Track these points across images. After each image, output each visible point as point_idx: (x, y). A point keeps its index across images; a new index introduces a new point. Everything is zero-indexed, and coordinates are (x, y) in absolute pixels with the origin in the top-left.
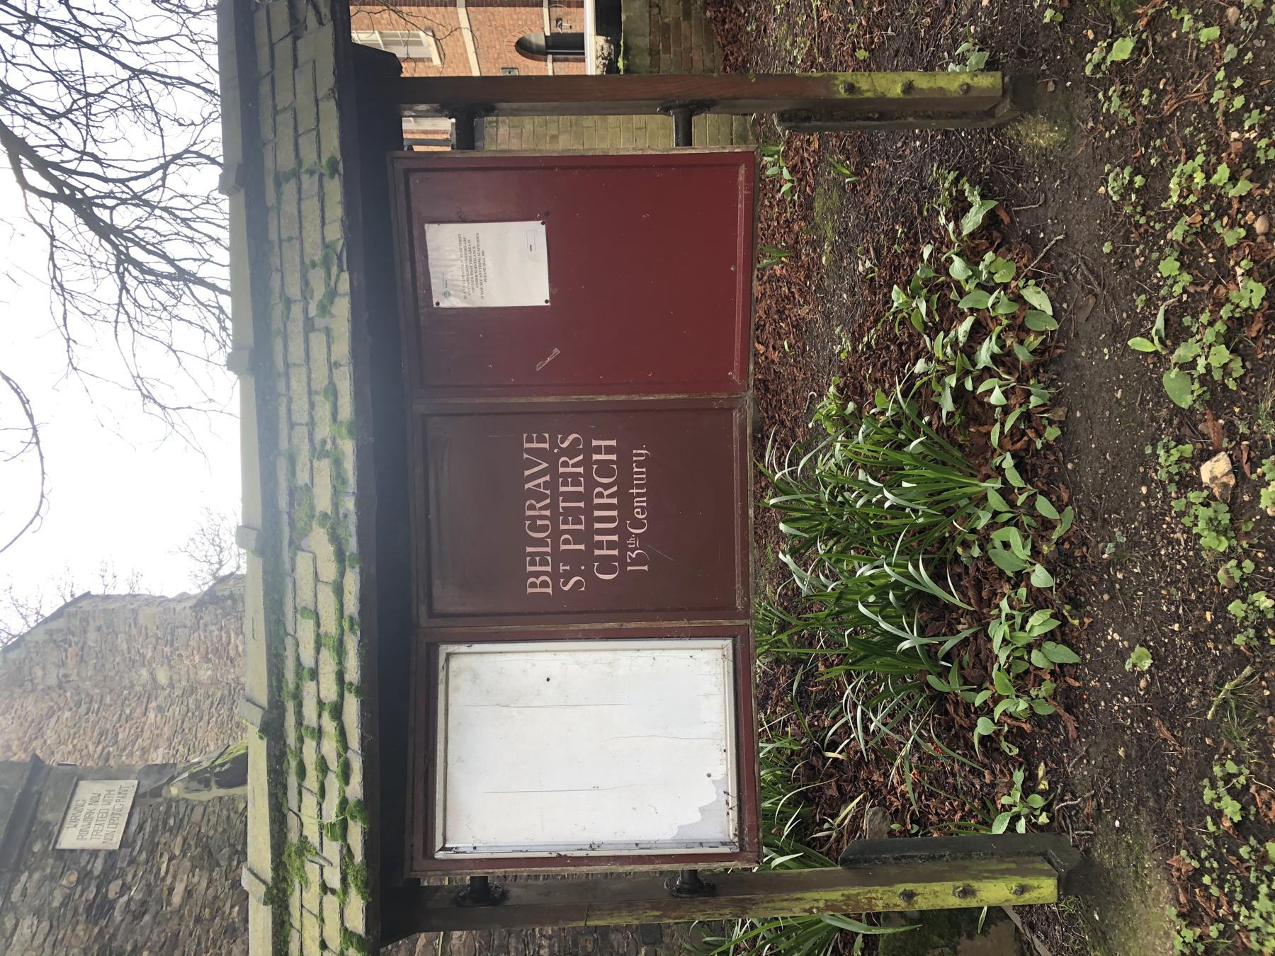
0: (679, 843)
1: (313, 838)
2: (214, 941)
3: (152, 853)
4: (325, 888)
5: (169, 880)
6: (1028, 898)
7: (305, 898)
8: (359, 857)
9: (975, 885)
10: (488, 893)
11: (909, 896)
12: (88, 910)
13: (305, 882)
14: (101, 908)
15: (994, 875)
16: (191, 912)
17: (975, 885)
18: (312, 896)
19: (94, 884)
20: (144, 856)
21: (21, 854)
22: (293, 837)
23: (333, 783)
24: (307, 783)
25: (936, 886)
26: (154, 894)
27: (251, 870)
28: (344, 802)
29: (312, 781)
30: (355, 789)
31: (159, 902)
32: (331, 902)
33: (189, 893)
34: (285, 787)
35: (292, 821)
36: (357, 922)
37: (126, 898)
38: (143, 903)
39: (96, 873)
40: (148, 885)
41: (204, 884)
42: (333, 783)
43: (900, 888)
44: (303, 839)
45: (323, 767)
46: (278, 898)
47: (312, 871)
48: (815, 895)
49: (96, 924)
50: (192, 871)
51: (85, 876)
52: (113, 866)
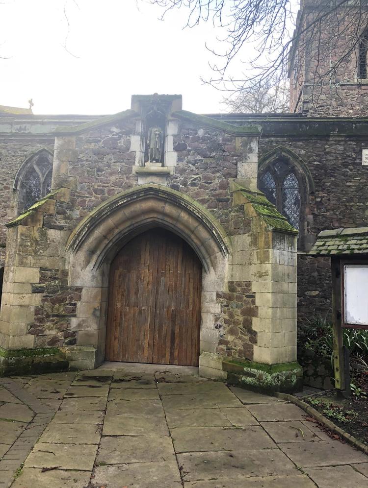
0: (346, 312)
1: (348, 243)
2: (336, 196)
3: (360, 174)
4: (339, 245)
5: (353, 181)
6: (336, 382)
7: (337, 241)
8: (344, 253)
9: (339, 371)
10: (338, 277)
11: (337, 358)
12: (346, 162)
13: (340, 241)
14: (346, 165)
15: (341, 376)
16: (344, 188)
17: (339, 371)
18: (337, 243)
19: (353, 162)
20: (360, 172)
21: (361, 140)
22: (349, 238)
23: (357, 247)
24: (358, 241)
25: (338, 363)
26: (348, 178)
27: (343, 230)
28: (353, 249)
29: (359, 242)
30: (356, 252)
31: (348, 179)
32: (335, 247)
33: (349, 186)
34: (358, 236)
35: (352, 238)
36: (333, 252)
37: (348, 170)
38: (347, 176)
39: (355, 161)
40: (352, 176)
41: (352, 190)
42: (357, 247)
43: (338, 356)
44: (348, 241)
45: (361, 244)
46: (337, 236)
47: (342, 243)
48: (337, 338)
49: (342, 165)
50: (356, 186)
51: (355, 159)
52: (357, 165)
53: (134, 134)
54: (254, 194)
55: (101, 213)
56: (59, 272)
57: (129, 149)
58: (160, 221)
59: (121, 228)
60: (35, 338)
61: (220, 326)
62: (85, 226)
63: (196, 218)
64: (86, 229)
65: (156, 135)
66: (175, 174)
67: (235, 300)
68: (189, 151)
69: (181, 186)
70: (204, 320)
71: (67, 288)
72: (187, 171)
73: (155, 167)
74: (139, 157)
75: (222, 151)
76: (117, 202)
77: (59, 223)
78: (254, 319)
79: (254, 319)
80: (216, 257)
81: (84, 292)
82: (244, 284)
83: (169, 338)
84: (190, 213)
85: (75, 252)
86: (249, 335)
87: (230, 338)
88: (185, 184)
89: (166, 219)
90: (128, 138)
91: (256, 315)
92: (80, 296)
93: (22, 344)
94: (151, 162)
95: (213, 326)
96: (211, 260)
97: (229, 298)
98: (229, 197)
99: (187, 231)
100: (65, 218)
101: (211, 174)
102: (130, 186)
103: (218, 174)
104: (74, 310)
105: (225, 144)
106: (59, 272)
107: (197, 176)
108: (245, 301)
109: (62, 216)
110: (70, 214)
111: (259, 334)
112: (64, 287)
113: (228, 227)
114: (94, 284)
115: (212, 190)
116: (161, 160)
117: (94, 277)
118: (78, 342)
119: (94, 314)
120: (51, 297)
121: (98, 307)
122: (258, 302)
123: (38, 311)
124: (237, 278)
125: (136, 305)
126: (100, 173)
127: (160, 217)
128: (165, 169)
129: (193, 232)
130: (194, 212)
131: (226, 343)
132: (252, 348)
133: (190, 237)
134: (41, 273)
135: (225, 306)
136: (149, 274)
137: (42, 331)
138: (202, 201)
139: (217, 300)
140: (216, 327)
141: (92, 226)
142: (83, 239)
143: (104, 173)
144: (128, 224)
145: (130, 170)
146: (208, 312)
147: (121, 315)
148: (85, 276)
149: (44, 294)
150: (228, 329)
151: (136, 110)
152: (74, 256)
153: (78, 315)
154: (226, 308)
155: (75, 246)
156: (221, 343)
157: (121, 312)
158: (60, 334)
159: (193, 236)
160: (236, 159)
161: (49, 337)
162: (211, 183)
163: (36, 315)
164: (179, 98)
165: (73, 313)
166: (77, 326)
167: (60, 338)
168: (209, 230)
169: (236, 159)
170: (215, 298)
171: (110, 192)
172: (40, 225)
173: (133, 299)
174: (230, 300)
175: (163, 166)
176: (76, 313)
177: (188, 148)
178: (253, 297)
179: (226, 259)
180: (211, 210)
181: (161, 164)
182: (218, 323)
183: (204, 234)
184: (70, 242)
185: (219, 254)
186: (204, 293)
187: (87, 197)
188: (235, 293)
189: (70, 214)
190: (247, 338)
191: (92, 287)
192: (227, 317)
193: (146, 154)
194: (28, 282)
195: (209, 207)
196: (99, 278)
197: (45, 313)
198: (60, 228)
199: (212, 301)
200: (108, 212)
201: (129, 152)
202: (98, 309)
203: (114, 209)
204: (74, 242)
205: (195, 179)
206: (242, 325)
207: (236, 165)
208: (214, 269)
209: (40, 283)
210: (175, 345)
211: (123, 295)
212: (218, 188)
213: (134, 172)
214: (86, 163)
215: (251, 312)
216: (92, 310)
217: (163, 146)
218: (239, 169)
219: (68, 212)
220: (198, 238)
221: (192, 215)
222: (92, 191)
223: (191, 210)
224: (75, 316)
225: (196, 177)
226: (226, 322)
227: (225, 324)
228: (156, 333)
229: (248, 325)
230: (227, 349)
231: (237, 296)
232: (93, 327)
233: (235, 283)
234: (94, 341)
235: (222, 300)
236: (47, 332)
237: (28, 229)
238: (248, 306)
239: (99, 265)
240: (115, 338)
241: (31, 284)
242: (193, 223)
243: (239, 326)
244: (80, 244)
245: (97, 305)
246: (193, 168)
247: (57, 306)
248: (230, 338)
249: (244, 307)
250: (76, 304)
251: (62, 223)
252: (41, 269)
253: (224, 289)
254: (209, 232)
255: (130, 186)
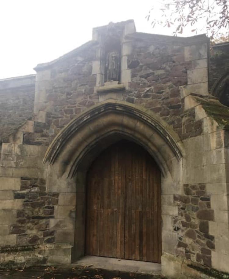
53: (95, 60)
54: (205, 98)
55: (71, 129)
56: (38, 181)
57: (90, 73)
58: (121, 132)
59: (89, 141)
60: (17, 237)
61: (178, 229)
62: (58, 140)
63: (154, 129)
64: (59, 144)
65: (112, 57)
66: (130, 89)
67: (190, 203)
68: (142, 67)
69: (135, 99)
70: (164, 222)
71: (46, 194)
72: (141, 85)
73: (114, 85)
74: (99, 79)
75: (171, 62)
76: (82, 118)
77: (38, 140)
78: (210, 223)
79: (210, 223)
80: (171, 162)
81: (60, 198)
82: (198, 186)
83: (137, 236)
84: (145, 123)
85: (52, 163)
86: (207, 240)
87: (188, 241)
88: (138, 96)
89: (126, 130)
90: (90, 64)
91: (212, 219)
92: (57, 201)
93: (5, 243)
94: (109, 81)
95: (172, 228)
96: (167, 165)
97: (185, 201)
98: (180, 103)
99: (144, 140)
100: (43, 136)
101: (162, 84)
102: (93, 104)
103: (169, 84)
104: (52, 213)
105: (175, 55)
106: (38, 181)
107: (149, 88)
108: (200, 203)
109: (39, 134)
110: (47, 133)
111: (216, 240)
112: (42, 193)
113: (181, 132)
114: (69, 190)
115: (164, 99)
116: (119, 79)
117: (69, 184)
118: (56, 240)
119: (70, 215)
120: (32, 201)
121: (74, 209)
122: (214, 205)
123: (20, 213)
124: (191, 183)
125: (109, 206)
126: (69, 97)
127: (120, 129)
128: (121, 86)
129: (149, 141)
130: (148, 121)
131: (185, 246)
132: (210, 253)
133: (147, 145)
134: (22, 182)
135: (182, 209)
136: (116, 180)
137: (24, 231)
138: (156, 110)
139: (174, 202)
140: (175, 230)
141: (63, 141)
142: (58, 152)
143: (72, 95)
144: (94, 137)
145: (92, 90)
146: (167, 214)
147: (98, 216)
148: (61, 183)
149: (24, 200)
150: (185, 231)
151: (96, 39)
152: (50, 167)
153: (56, 217)
154: (183, 211)
155: (51, 158)
156: (180, 245)
157: (97, 213)
158: (40, 233)
159: (150, 144)
160: (185, 68)
161: (30, 236)
162: (162, 92)
163: (18, 217)
164: (131, 22)
165: (51, 214)
166: (54, 226)
167: (40, 237)
168: (163, 136)
169: (185, 68)
170: (172, 200)
171: (78, 110)
172: (20, 142)
173: (106, 201)
174: (186, 203)
175: (119, 83)
176: (54, 215)
177: (141, 64)
178: (208, 199)
179: (181, 163)
180: (164, 117)
181: (117, 82)
182: (176, 225)
183: (158, 141)
184: (46, 154)
185: (174, 158)
186: (163, 196)
187: (60, 117)
188: (190, 196)
189: (47, 133)
190: (204, 242)
191: (68, 193)
192: (184, 220)
193: (106, 77)
194: (10, 190)
195: (162, 115)
196: (74, 185)
197: (26, 215)
198: (39, 144)
199: (170, 204)
200: (76, 128)
201: (91, 75)
202: (74, 211)
203: (80, 126)
204: (50, 156)
205: (148, 91)
206: (198, 228)
207: (186, 72)
208: (171, 173)
209: (20, 191)
210: (144, 242)
211: (98, 199)
212: (169, 96)
213: (95, 92)
214: (58, 89)
215: (207, 216)
216: (68, 212)
217: (119, 67)
218: (189, 76)
219: (45, 131)
220: (154, 145)
221: (147, 125)
222: (64, 112)
223: (145, 119)
224: (53, 217)
225: (148, 89)
226: (184, 224)
227: (183, 226)
228: (127, 232)
229: (204, 228)
230: (186, 252)
231: (192, 199)
232: (70, 227)
233: (189, 185)
234: (72, 238)
235: (179, 202)
236: (29, 232)
237: (9, 146)
238: (204, 209)
239: (74, 174)
240: (93, 236)
241: (14, 191)
242: (148, 132)
243: (196, 229)
244: (55, 157)
245: (72, 208)
246: (146, 81)
247: (37, 210)
248: (188, 241)
249: (200, 210)
250: (53, 207)
251: (40, 139)
252: (22, 178)
253: (180, 192)
254: (162, 138)
255: (93, 104)
